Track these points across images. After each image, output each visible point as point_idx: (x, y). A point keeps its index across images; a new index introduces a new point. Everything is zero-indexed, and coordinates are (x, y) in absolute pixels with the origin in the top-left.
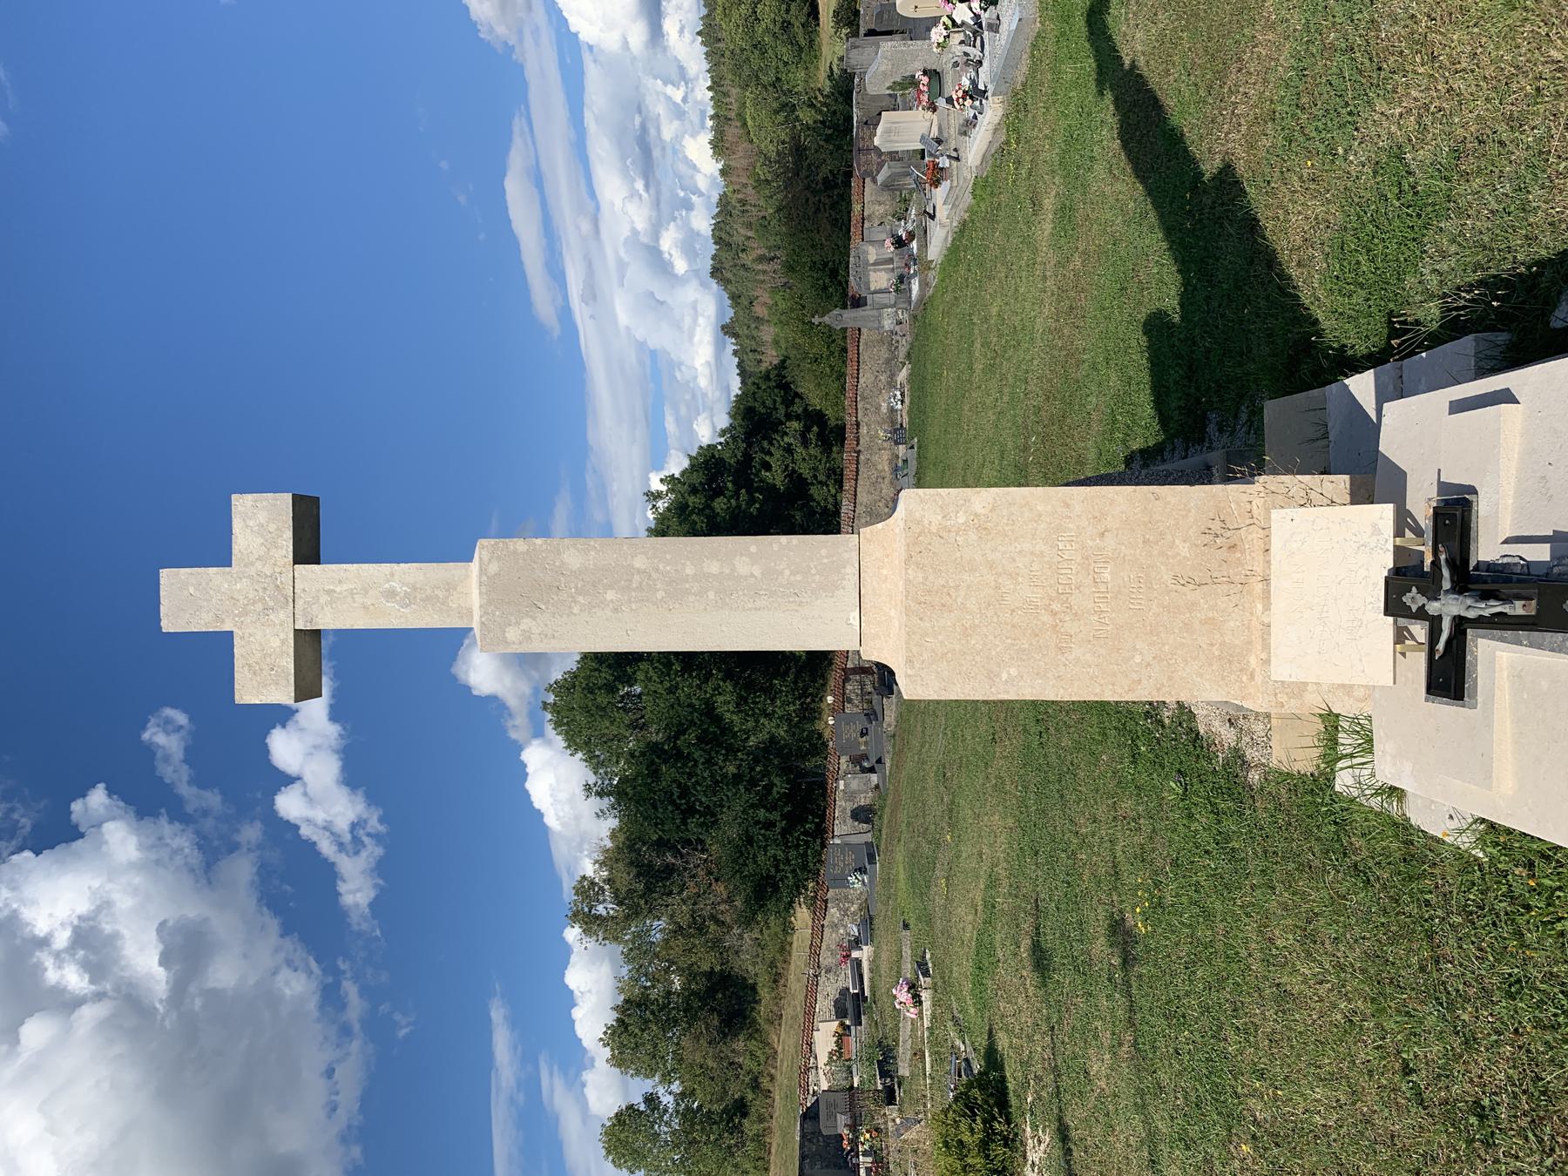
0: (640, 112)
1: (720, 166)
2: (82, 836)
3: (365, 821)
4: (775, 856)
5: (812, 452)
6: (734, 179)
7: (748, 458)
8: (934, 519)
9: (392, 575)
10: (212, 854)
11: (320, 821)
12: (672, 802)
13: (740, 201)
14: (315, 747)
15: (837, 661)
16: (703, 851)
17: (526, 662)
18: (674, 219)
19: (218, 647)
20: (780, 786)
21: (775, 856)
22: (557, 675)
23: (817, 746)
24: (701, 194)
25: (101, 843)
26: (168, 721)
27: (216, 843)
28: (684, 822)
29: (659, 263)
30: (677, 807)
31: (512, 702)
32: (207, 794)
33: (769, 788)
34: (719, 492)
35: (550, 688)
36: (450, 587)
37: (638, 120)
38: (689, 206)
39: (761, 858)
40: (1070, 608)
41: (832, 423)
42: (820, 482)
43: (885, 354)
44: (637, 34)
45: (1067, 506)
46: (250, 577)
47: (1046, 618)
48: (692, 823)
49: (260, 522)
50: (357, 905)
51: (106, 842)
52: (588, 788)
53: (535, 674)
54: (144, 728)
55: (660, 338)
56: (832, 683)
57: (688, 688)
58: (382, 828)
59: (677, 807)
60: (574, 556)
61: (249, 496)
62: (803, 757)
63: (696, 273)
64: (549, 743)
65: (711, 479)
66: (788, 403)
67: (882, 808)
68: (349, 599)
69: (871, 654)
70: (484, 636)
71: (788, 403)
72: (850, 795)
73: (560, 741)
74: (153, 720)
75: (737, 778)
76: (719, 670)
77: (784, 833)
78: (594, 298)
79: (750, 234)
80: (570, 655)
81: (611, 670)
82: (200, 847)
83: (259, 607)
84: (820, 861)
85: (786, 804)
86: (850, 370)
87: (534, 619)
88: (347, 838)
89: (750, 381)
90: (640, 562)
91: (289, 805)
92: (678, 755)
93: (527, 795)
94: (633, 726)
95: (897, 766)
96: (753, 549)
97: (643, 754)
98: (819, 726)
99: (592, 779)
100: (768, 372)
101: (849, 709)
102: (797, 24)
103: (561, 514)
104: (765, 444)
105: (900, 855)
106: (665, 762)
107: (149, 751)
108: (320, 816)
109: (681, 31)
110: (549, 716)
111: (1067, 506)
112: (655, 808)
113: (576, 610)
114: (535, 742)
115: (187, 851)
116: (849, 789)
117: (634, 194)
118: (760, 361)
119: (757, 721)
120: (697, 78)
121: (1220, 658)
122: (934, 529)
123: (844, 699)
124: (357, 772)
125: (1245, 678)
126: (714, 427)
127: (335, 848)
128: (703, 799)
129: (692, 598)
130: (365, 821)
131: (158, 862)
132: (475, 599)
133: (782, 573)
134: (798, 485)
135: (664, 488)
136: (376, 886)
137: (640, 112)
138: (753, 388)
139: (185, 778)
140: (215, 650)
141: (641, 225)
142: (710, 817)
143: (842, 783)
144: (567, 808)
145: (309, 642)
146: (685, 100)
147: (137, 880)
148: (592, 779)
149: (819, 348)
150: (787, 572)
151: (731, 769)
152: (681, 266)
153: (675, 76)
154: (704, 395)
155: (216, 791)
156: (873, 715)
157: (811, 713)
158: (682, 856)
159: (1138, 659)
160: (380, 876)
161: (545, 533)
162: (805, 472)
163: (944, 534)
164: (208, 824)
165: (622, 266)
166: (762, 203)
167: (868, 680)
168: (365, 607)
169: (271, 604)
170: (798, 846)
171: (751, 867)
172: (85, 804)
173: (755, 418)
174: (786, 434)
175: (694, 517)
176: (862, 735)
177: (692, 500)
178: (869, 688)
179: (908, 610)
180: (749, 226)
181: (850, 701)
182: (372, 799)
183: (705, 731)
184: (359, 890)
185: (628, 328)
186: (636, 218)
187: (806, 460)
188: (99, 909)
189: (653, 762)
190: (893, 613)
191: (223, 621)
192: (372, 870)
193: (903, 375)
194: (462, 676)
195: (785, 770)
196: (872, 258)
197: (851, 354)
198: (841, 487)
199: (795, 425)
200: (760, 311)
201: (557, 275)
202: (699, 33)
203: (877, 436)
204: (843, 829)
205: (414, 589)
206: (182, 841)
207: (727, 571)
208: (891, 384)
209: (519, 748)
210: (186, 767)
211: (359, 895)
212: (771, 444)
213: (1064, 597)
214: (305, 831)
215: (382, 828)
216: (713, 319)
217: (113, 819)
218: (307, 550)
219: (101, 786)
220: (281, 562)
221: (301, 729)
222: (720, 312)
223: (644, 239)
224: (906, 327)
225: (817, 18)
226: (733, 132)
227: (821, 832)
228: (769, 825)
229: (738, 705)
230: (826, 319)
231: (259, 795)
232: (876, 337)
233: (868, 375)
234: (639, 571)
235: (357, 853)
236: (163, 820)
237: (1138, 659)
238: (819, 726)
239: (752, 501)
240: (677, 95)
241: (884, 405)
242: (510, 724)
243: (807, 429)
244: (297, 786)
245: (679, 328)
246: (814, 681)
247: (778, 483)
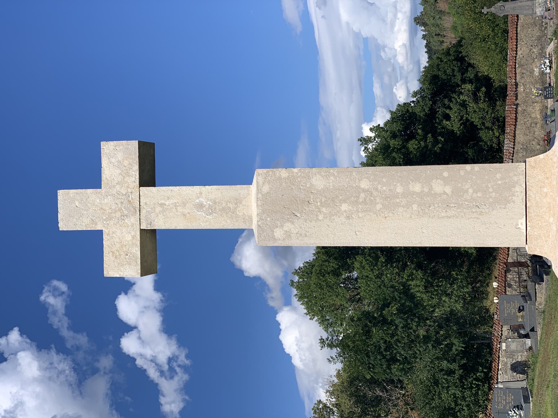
2: (5, 360)
3: (177, 357)
4: (454, 394)
5: (481, 106)
7: (433, 112)
10: (82, 377)
11: (149, 357)
12: (381, 353)
14: (145, 307)
15: (501, 257)
16: (402, 388)
17: (280, 253)
19: (93, 239)
20: (458, 345)
21: (454, 394)
22: (299, 264)
23: (486, 318)
25: (17, 365)
26: (56, 289)
27: (85, 368)
28: (389, 367)
30: (384, 357)
31: (270, 281)
32: (79, 336)
33: (450, 346)
34: (412, 136)
35: (296, 272)
36: (238, 201)
39: (444, 396)
41: (496, 84)
42: (487, 128)
43: (536, 32)
46: (112, 195)
48: (395, 368)
49: (119, 159)
50: (172, 412)
51: (20, 365)
52: (322, 341)
53: (285, 263)
54: (41, 293)
55: (370, 29)
56: (496, 273)
57: (390, 274)
58: (187, 362)
59: (384, 357)
60: (319, 180)
62: (475, 325)
64: (295, 309)
65: (406, 128)
66: (463, 71)
67: (534, 363)
68: (174, 210)
69: (533, 249)
70: (259, 234)
71: (463, 71)
72: (510, 353)
73: (302, 309)
74: (46, 288)
75: (427, 339)
76: (412, 262)
77: (461, 378)
80: (308, 248)
81: (337, 259)
82: (75, 370)
83: (118, 214)
84: (488, 400)
85: (462, 358)
86: (511, 45)
87: (293, 223)
88: (166, 367)
89: (435, 57)
90: (364, 184)
91: (129, 344)
92: (385, 321)
93: (280, 344)
94: (351, 300)
95: (547, 334)
96: (446, 174)
97: (359, 319)
98: (486, 303)
99: (325, 336)
100: (449, 49)
101: (509, 291)
103: (302, 153)
104: (446, 101)
105: (548, 397)
106: (375, 325)
107: (44, 308)
108: (148, 352)
110: (295, 292)
112: (369, 357)
113: (321, 217)
114: (286, 309)
115: (67, 372)
116: (509, 348)
118: (443, 42)
119: (440, 299)
123: (506, 285)
124: (173, 323)
126: (408, 90)
127: (158, 374)
128: (401, 352)
129: (401, 209)
130: (177, 357)
131: (50, 378)
132: (254, 210)
133: (467, 191)
134: (471, 131)
135: (372, 135)
136: (184, 400)
138: (438, 62)
139: (66, 325)
140: (90, 243)
142: (408, 365)
143: (504, 345)
144: (307, 354)
145: (149, 236)
147: (38, 389)
148: (325, 336)
149: (487, 30)
150: (471, 191)
151: (422, 332)
154: (402, 68)
155: (85, 334)
156: (527, 296)
157: (479, 294)
158: (387, 391)
160: (187, 393)
161: (290, 165)
162: (476, 121)
164: (80, 356)
167: (524, 271)
168: (184, 215)
169: (126, 212)
170: (471, 388)
171: (437, 401)
172: (7, 340)
173: (438, 84)
175: (394, 154)
176: (520, 310)
177: (392, 143)
178: (525, 277)
181: (510, 286)
182: (181, 343)
183: (403, 305)
184: (173, 402)
185: (348, 23)
187: (477, 112)
188: (16, 406)
189: (366, 325)
190: (551, 220)
191: (96, 224)
192: (181, 390)
193: (550, 48)
194: (237, 263)
195: (461, 334)
197: (511, 30)
198: (503, 132)
199: (468, 86)
203: (531, 93)
204: (504, 377)
205: (215, 203)
206: (65, 366)
207: (426, 190)
208: (542, 55)
209: (275, 312)
210: (66, 318)
211: (173, 405)
212: (450, 101)
214: (139, 362)
215: (187, 362)
216: (408, 14)
217: (24, 350)
218: (148, 178)
219: (16, 329)
220: (131, 185)
221: (137, 296)
222: (414, 8)
224: (553, 13)
227: (488, 379)
228: (450, 372)
229: (426, 287)
230: (493, 9)
231: (111, 338)
232: (531, 21)
233: (524, 49)
234: (364, 191)
235: (172, 378)
236: (53, 352)
238: (486, 303)
239: (436, 142)
241: (536, 70)
242: (269, 295)
243: (478, 89)
244: (134, 332)
245: (384, 21)
246: (482, 271)
247: (455, 129)
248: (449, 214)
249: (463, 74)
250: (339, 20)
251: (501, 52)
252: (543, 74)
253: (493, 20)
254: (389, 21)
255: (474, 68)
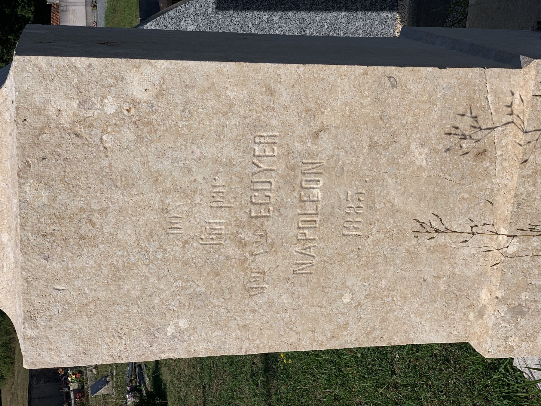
8: (66, 107)
40: (264, 236)
45: (271, 92)
47: (232, 251)
111: (271, 92)
121: (446, 293)
122: (65, 121)
125: (472, 316)
159: (346, 299)
163: (82, 131)
179: (24, 247)
213: (258, 222)
237: (346, 299)
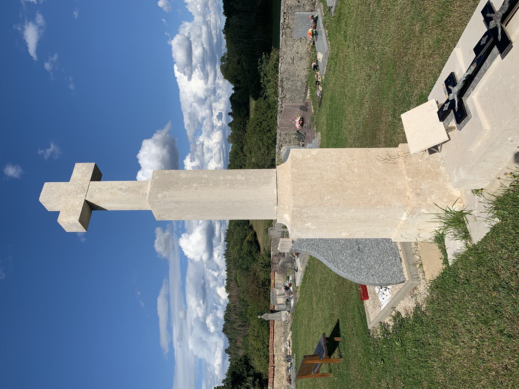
0: (203, 278)
1: (228, 295)
6: (232, 299)
8: (300, 156)
9: (122, 184)
13: (234, 306)
18: (212, 313)
24: (221, 305)
29: (204, 327)
37: (203, 281)
38: (217, 309)
41: (264, 378)
43: (283, 330)
44: (205, 257)
45: (341, 153)
55: (203, 354)
61: (81, 163)
63: (218, 332)
71: (248, 370)
78: (182, 339)
79: (236, 317)
86: (271, 335)
87: (168, 191)
102: (254, 252)
109: (219, 255)
111: (341, 153)
117: (199, 305)
120: (222, 269)
122: (300, 159)
129: (221, 186)
137: (203, 278)
141: (200, 315)
146: (218, 276)
150: (253, 179)
152: (212, 329)
153: (215, 267)
159: (370, 194)
165: (192, 328)
166: (241, 307)
174: (247, 382)
180: (236, 314)
185: (192, 350)
186: (199, 312)
196: (278, 293)
197: (271, 330)
199: (251, 378)
200: (239, 344)
201: (170, 329)
202: (224, 255)
216: (222, 348)
222: (225, 345)
223: (201, 320)
225: (260, 250)
226: (232, 284)
230: (262, 317)
232: (280, 324)
234: (205, 178)
237: (370, 194)
240: (216, 274)
248: (243, 187)
249: (248, 372)
250: (188, 348)
251: (266, 358)
252: (286, 350)
253: (263, 321)
254: (212, 351)
255: (253, 369)
